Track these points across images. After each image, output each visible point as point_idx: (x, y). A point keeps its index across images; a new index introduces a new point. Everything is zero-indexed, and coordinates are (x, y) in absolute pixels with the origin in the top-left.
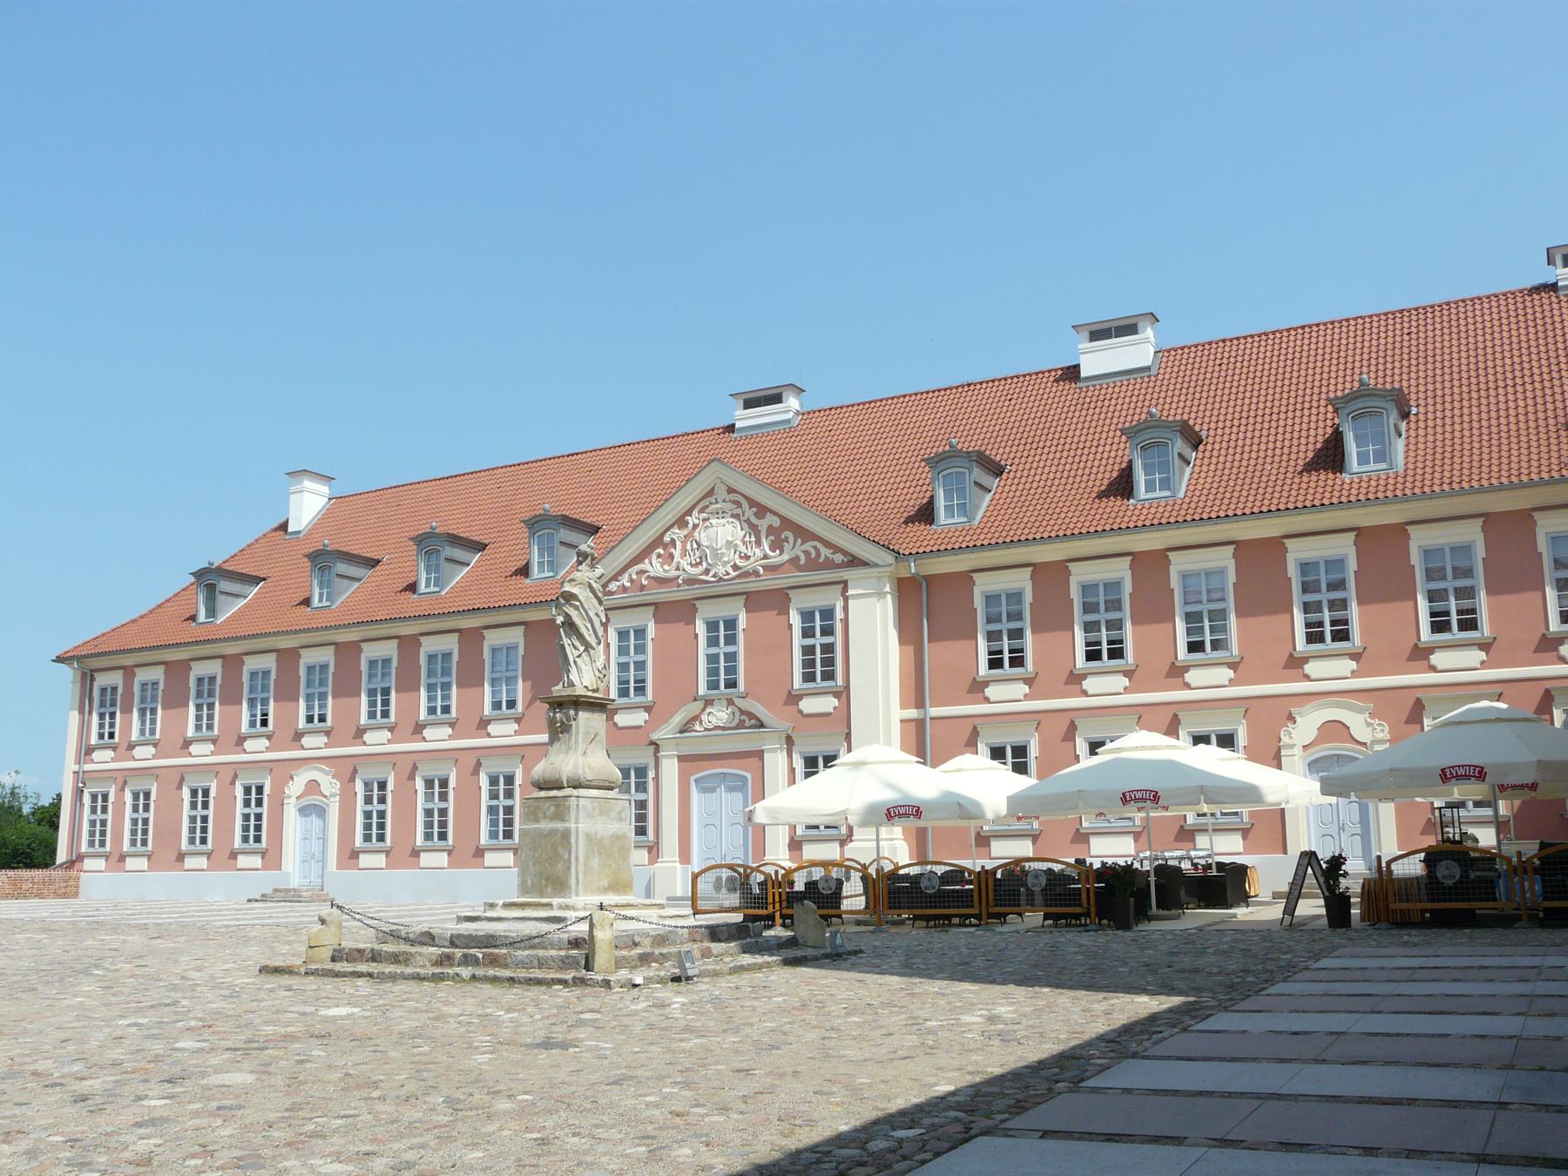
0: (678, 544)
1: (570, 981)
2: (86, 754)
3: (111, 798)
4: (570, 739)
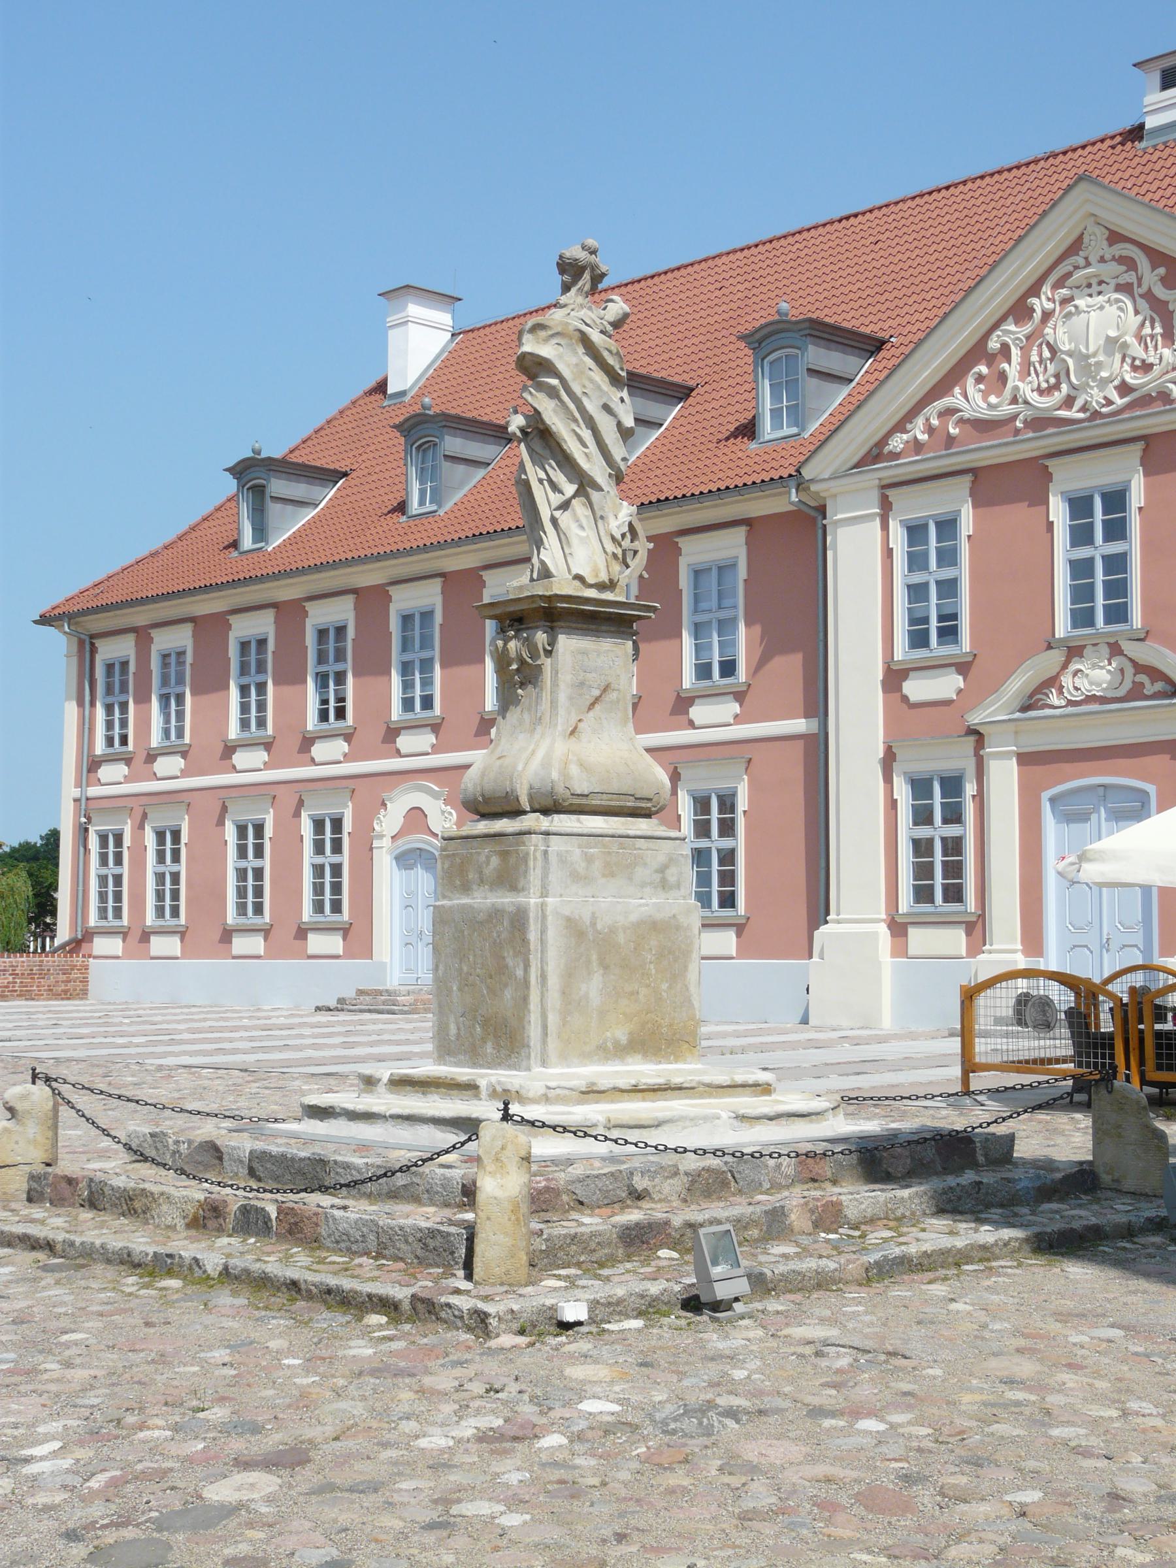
0: (1015, 353)
1: (406, 1306)
2: (89, 771)
3: (127, 841)
4: (539, 697)
